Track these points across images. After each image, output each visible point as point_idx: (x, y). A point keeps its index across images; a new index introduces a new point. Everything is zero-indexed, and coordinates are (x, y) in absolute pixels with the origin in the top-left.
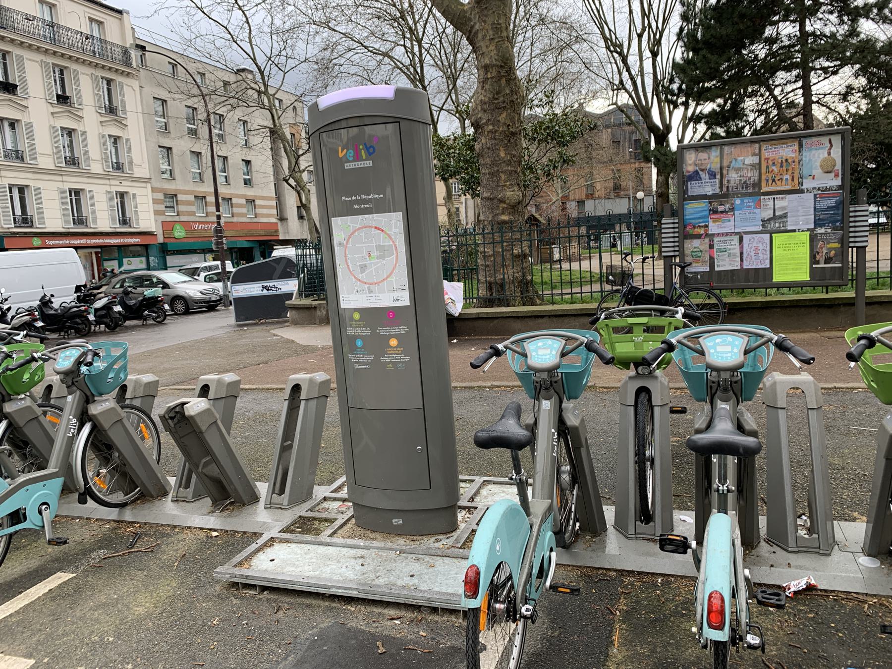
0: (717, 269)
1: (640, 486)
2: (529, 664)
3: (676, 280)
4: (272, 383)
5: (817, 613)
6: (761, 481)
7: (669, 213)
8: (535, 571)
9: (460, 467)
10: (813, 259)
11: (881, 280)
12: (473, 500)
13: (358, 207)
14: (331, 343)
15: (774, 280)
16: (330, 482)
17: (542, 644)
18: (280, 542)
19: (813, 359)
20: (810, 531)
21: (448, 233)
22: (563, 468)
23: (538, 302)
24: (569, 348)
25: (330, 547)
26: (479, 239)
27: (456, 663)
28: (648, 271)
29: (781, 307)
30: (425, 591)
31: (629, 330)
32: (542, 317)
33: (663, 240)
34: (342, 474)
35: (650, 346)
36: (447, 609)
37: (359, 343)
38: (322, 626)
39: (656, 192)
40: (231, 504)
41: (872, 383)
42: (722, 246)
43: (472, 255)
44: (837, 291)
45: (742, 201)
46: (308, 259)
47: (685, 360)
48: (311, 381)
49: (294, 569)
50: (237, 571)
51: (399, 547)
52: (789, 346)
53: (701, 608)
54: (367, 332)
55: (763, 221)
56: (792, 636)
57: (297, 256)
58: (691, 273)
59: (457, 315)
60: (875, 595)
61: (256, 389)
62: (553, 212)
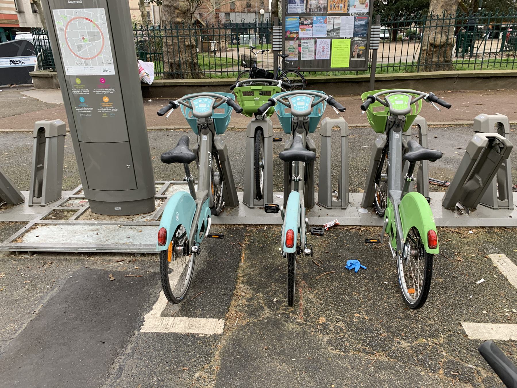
0: (302, 59)
1: (256, 181)
2: (197, 276)
3: (280, 65)
4: (26, 128)
5: (338, 237)
6: (316, 175)
7: (277, 24)
8: (199, 228)
9: (155, 176)
10: (352, 56)
11: (383, 68)
12: (164, 194)
13: (73, 2)
14: (62, 102)
15: (331, 67)
16: (73, 188)
17: (204, 265)
18: (42, 225)
19: (345, 109)
20: (338, 198)
21: (142, 28)
22: (215, 173)
23: (202, 76)
24: (217, 103)
25: (76, 226)
26: (163, 33)
27: (157, 280)
28: (265, 60)
29: (334, 82)
30: (136, 245)
31: (252, 93)
32: (204, 86)
33: (274, 40)
34: (80, 183)
35: (262, 102)
36: (150, 253)
37: (82, 100)
38: (74, 270)
39: (271, 10)
40: (4, 205)
41: (372, 122)
42: (306, 45)
43: (160, 44)
44: (362, 74)
45: (317, 19)
46: (43, 42)
47: (281, 111)
48: (52, 125)
49: (53, 240)
50: (13, 245)
51: (120, 223)
52: (334, 102)
53: (284, 240)
54: (87, 92)
55: (328, 31)
56: (326, 248)
57: (34, 39)
58: (288, 61)
59: (150, 84)
60: (365, 226)
61: (14, 131)
62: (210, 19)
